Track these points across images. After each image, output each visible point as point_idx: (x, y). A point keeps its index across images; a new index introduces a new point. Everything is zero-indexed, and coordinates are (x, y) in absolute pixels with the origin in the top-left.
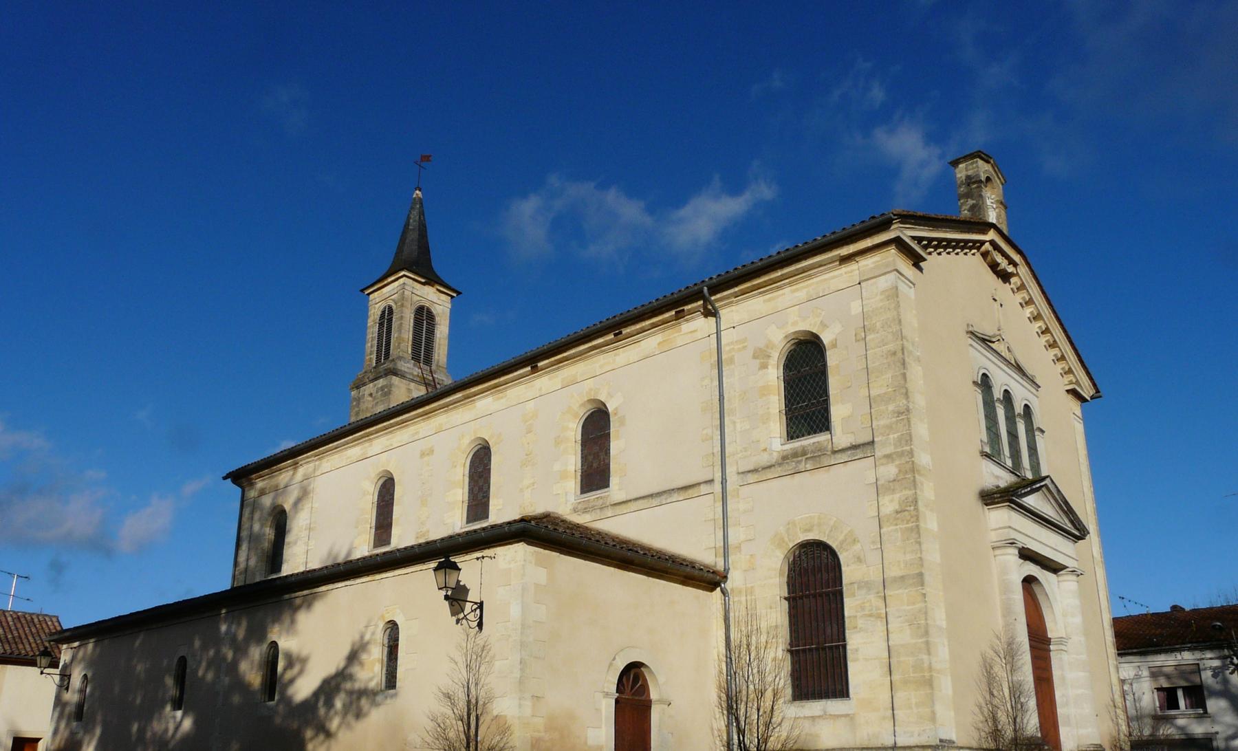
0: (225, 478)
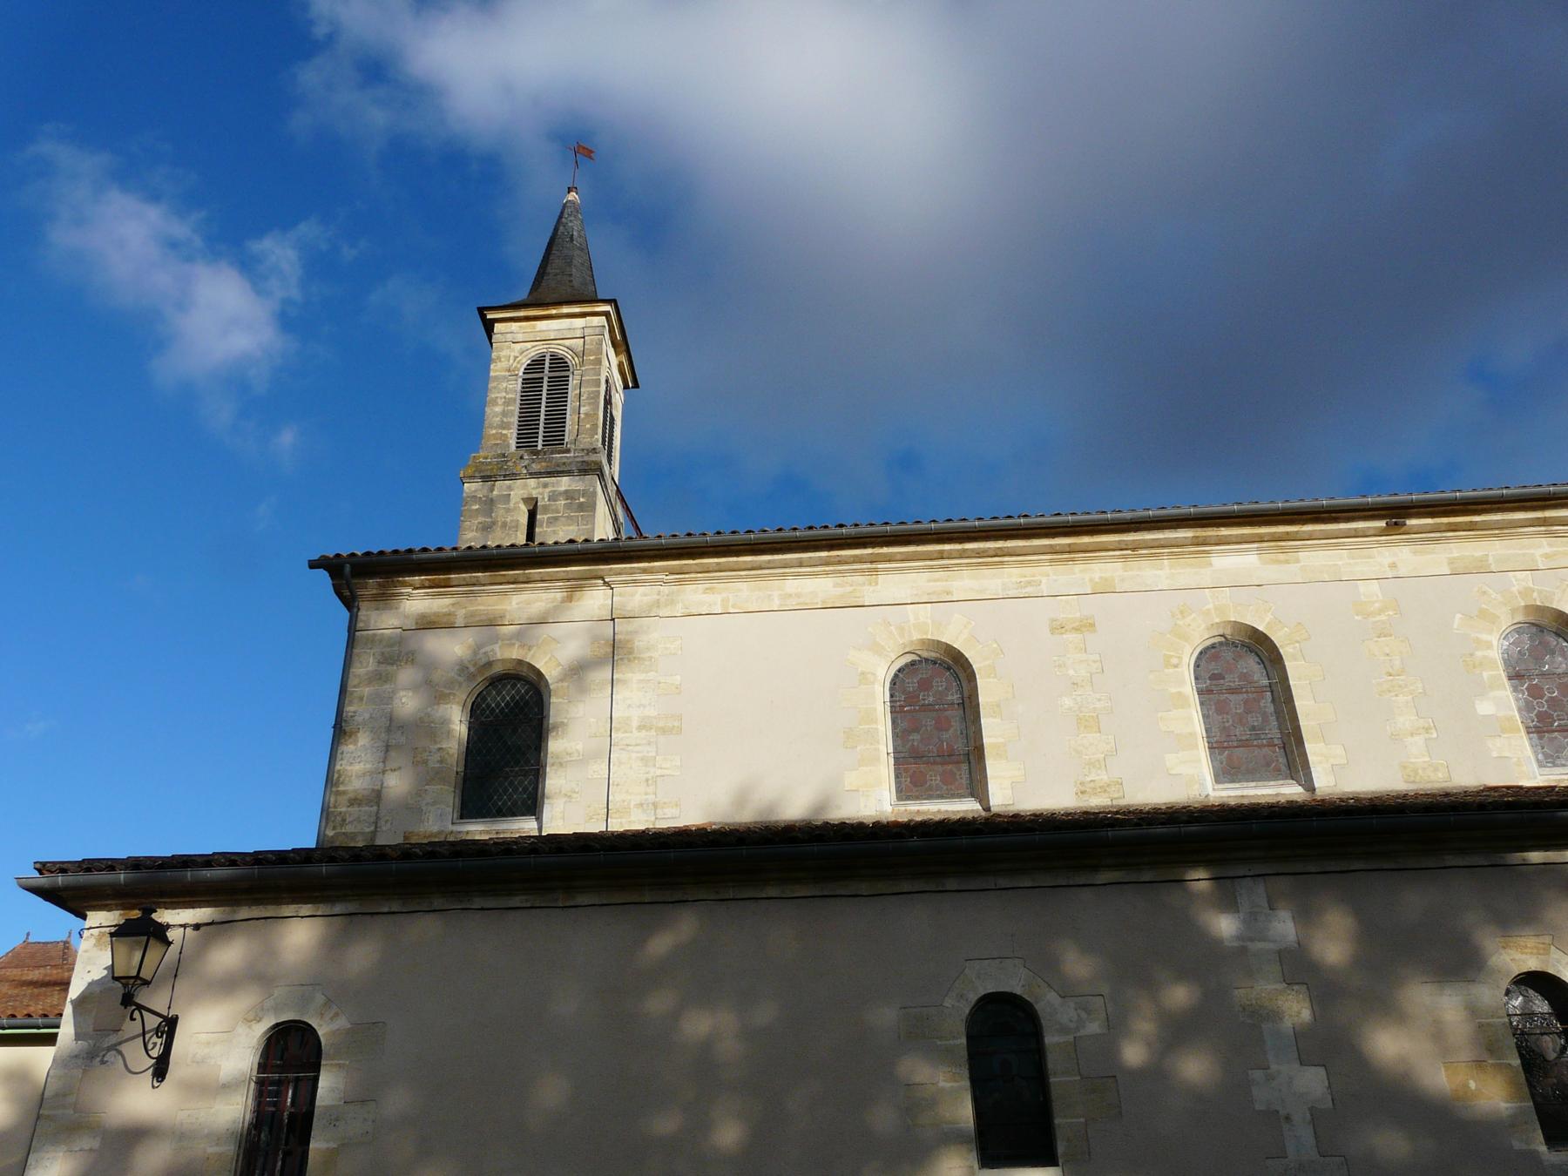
0: (313, 565)
